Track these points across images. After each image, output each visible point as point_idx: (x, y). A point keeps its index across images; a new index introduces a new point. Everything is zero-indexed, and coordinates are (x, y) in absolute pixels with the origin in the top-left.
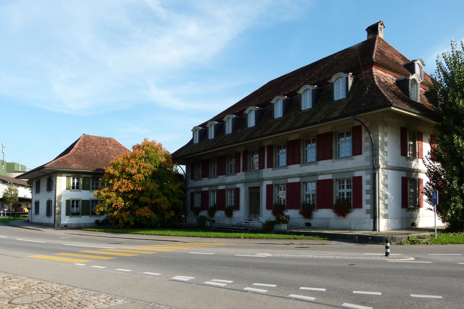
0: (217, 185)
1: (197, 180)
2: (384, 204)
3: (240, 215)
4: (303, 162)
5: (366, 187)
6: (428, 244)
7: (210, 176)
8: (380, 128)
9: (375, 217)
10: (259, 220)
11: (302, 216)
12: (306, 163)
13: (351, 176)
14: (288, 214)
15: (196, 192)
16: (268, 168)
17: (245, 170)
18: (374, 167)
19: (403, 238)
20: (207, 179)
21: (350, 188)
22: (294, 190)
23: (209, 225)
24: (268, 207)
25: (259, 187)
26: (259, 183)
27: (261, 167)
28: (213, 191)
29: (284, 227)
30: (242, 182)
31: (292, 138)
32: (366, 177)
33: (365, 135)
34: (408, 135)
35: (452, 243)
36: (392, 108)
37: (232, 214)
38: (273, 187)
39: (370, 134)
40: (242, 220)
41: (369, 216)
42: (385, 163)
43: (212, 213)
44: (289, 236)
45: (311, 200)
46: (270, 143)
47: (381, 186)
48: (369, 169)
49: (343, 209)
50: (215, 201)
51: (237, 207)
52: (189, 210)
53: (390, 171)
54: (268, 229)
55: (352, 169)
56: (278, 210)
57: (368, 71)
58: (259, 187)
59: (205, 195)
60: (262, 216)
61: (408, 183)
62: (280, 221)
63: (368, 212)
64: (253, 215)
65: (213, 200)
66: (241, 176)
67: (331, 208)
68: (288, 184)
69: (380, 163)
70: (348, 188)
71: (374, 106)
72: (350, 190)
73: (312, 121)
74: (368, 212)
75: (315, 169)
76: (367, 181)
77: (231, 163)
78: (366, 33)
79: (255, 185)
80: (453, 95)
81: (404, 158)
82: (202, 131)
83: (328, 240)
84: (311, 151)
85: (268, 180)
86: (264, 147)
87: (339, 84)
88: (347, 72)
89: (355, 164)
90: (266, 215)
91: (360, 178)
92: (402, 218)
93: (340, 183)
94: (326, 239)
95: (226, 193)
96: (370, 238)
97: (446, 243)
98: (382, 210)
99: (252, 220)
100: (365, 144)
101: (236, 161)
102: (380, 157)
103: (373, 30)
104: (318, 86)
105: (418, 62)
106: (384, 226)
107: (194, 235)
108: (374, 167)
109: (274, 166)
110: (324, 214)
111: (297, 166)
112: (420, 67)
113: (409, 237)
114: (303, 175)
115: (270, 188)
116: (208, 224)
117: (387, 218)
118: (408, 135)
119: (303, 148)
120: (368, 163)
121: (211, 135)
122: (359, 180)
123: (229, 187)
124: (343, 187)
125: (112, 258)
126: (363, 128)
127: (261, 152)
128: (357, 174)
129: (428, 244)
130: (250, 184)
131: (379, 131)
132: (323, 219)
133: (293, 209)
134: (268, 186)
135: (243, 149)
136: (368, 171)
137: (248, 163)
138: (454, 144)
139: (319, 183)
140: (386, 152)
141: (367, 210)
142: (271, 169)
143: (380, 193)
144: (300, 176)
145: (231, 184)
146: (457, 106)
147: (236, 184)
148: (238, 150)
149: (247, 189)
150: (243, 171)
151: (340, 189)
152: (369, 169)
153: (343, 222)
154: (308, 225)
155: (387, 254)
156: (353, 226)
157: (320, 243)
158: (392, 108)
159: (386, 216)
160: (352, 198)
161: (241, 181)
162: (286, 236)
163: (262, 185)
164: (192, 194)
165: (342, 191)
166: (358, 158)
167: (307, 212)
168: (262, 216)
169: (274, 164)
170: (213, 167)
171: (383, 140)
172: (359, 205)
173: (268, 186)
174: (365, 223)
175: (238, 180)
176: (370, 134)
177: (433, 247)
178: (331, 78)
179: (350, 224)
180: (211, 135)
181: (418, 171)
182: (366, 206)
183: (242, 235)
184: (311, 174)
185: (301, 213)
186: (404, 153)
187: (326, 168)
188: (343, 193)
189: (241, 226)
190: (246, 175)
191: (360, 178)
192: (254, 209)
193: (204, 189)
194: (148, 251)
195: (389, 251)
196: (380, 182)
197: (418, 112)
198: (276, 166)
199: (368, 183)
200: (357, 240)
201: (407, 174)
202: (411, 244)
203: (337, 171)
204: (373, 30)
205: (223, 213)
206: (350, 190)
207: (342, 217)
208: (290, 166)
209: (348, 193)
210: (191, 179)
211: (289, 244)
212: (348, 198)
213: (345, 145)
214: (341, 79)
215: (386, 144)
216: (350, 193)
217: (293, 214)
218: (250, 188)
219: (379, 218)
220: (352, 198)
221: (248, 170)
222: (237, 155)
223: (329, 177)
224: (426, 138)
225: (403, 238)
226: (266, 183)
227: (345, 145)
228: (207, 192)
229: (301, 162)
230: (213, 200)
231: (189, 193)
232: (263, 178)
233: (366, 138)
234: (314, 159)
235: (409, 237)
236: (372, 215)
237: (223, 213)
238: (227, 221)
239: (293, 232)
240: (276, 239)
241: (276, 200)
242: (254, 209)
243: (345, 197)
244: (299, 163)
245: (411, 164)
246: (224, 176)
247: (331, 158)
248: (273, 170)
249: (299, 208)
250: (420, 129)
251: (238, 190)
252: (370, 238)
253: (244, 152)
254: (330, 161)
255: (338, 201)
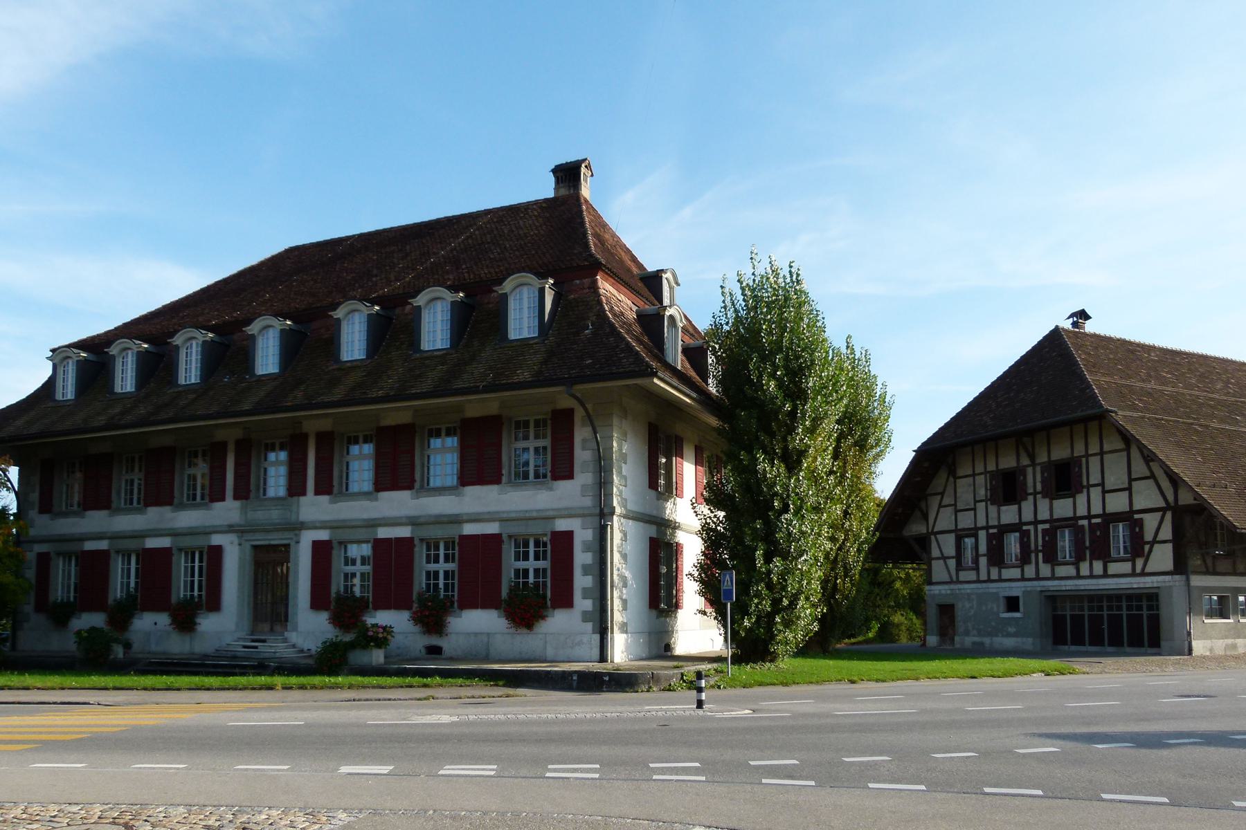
0: (142, 535)
1: (66, 515)
2: (621, 598)
3: (223, 627)
4: (422, 487)
5: (582, 558)
6: (719, 687)
7: (114, 505)
8: (616, 421)
9: (603, 630)
10: (285, 641)
11: (417, 629)
12: (427, 489)
13: (548, 530)
14: (388, 620)
15: (59, 554)
16: (317, 493)
17: (242, 493)
18: (601, 510)
19: (672, 677)
20: (104, 513)
21: (453, 561)
22: (392, 560)
23: (121, 655)
24: (319, 601)
25: (287, 546)
26: (287, 535)
27: (296, 488)
28: (127, 555)
29: (377, 657)
30: (230, 529)
31: (389, 421)
32: (583, 535)
33: (581, 434)
34: (661, 444)
35: (761, 684)
36: (656, 381)
37: (195, 624)
38: (332, 548)
39: (595, 433)
40: (228, 639)
41: (589, 626)
42: (624, 503)
43: (122, 616)
44: (408, 680)
45: (441, 586)
46: (325, 425)
47: (617, 556)
48: (590, 515)
49: (526, 610)
50: (132, 585)
51: (213, 603)
52: (29, 609)
53: (631, 522)
54: (330, 663)
55: (551, 513)
56: (347, 612)
57: (587, 281)
58: (287, 546)
59: (94, 567)
60: (295, 629)
61: (661, 551)
62: (369, 642)
63: (586, 617)
64: (266, 627)
65: (122, 579)
66: (228, 510)
67: (496, 608)
68: (464, 539)
69: (615, 503)
70: (537, 558)
71: (614, 369)
72: (451, 566)
73: (459, 384)
74: (586, 617)
75: (448, 502)
76: (584, 542)
77: (192, 471)
78: (551, 179)
79: (275, 539)
80: (758, 368)
81: (653, 493)
82: (92, 358)
83: (504, 686)
84: (443, 458)
85: (316, 528)
86: (305, 437)
87: (521, 299)
88: (543, 276)
89: (555, 502)
90: (311, 628)
91: (569, 535)
92: (650, 633)
93: (428, 549)
94: (501, 683)
95: (174, 559)
96: (607, 678)
97: (751, 686)
98: (618, 615)
99: (264, 641)
100: (582, 455)
101: (212, 469)
102: (615, 490)
103: (568, 174)
104: (466, 296)
105: (668, 275)
106: (621, 650)
107: (118, 685)
108: (601, 510)
109: (335, 490)
110: (476, 624)
111: (403, 496)
112: (671, 288)
113: (682, 675)
114: (422, 520)
115: (322, 551)
116: (119, 652)
117: (626, 632)
118: (661, 444)
119: (423, 449)
120: (588, 502)
121: (125, 379)
122: (564, 541)
123: (187, 542)
124: (526, 558)
125: (26, 747)
126: (579, 414)
127: (296, 445)
128: (562, 525)
129: (719, 687)
130: (258, 536)
131: (615, 428)
132: (476, 634)
133: (476, 607)
134: (318, 546)
135: (238, 433)
136: (589, 519)
137: (253, 476)
138: (756, 472)
139: (381, 546)
140: (625, 478)
141: (585, 613)
142: (324, 499)
143: (615, 572)
144: (413, 522)
145: (192, 532)
146: (764, 391)
147: (210, 533)
148: (220, 436)
149: (247, 546)
150: (236, 497)
151: (428, 562)
152: (590, 515)
153: (527, 641)
154: (434, 651)
155: (700, 704)
156: (550, 653)
157: (500, 693)
158: (656, 381)
159: (624, 628)
160: (549, 585)
161: (230, 526)
162: (374, 680)
163: (298, 542)
164: (44, 559)
165: (522, 565)
166: (563, 485)
167: (432, 618)
168: (295, 629)
169: (335, 483)
170: (128, 480)
171: (620, 449)
172: (565, 600)
173: (318, 546)
174: (580, 643)
175: (218, 522)
176: (595, 433)
177: (731, 692)
178: (504, 279)
179: (545, 648)
180: (125, 379)
181: (674, 526)
182: (583, 604)
183: (278, 680)
184: (445, 519)
185: (417, 619)
186: (653, 484)
187: (487, 507)
188: (526, 572)
189: (234, 657)
190: (244, 510)
191: (569, 535)
192: (270, 607)
193: (89, 546)
194: (107, 726)
195: (703, 696)
196: (615, 548)
197: (694, 395)
198: (340, 493)
199: (587, 548)
200: (575, 684)
201: (658, 531)
202: (689, 689)
203: (513, 515)
204: (568, 174)
205: (163, 619)
206: (451, 566)
207: (525, 631)
208: (385, 495)
209: (536, 571)
210: (42, 511)
211: (425, 699)
212: (536, 584)
213: (527, 449)
214: (525, 289)
215: (624, 458)
216: (453, 572)
217: (395, 620)
218: (255, 547)
219: (612, 632)
220: (549, 585)
221: (252, 495)
222: (216, 453)
223: (492, 528)
224: (689, 452)
225: (672, 677)
226: (308, 538)
227: (527, 449)
228: (103, 556)
229: (417, 485)
230: (122, 579)
231: (31, 556)
232: (302, 523)
233: (584, 441)
234: (452, 480)
235: (682, 675)
236: (598, 625)
237: (163, 619)
238: (177, 645)
239: (400, 670)
240: (374, 687)
241: (338, 585)
242: (270, 607)
243: (531, 579)
244: (410, 487)
245: (665, 509)
246: (168, 508)
247: (497, 480)
248: (332, 502)
249: (408, 608)
250: (679, 429)
251: (216, 554)
252: (607, 678)
253: (239, 443)
254: (495, 488)
255: (514, 590)
